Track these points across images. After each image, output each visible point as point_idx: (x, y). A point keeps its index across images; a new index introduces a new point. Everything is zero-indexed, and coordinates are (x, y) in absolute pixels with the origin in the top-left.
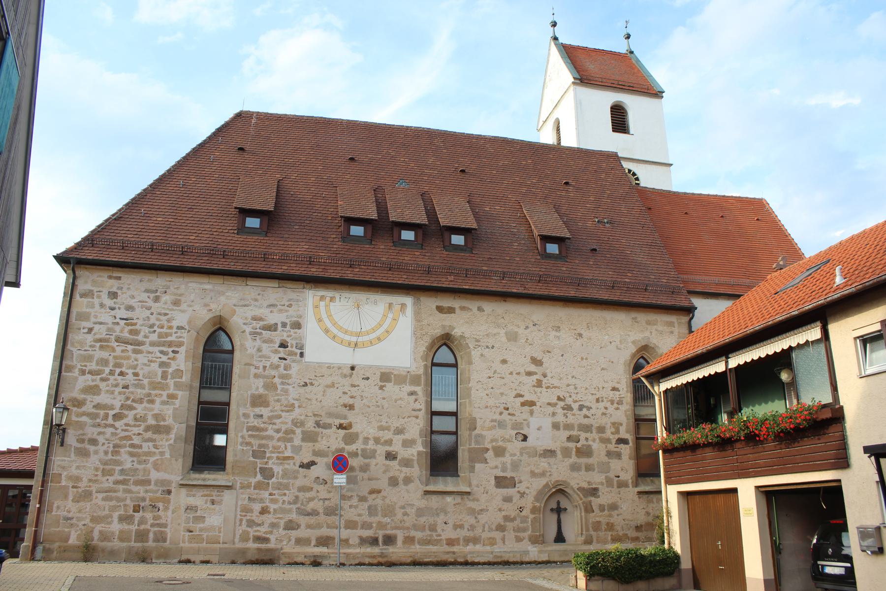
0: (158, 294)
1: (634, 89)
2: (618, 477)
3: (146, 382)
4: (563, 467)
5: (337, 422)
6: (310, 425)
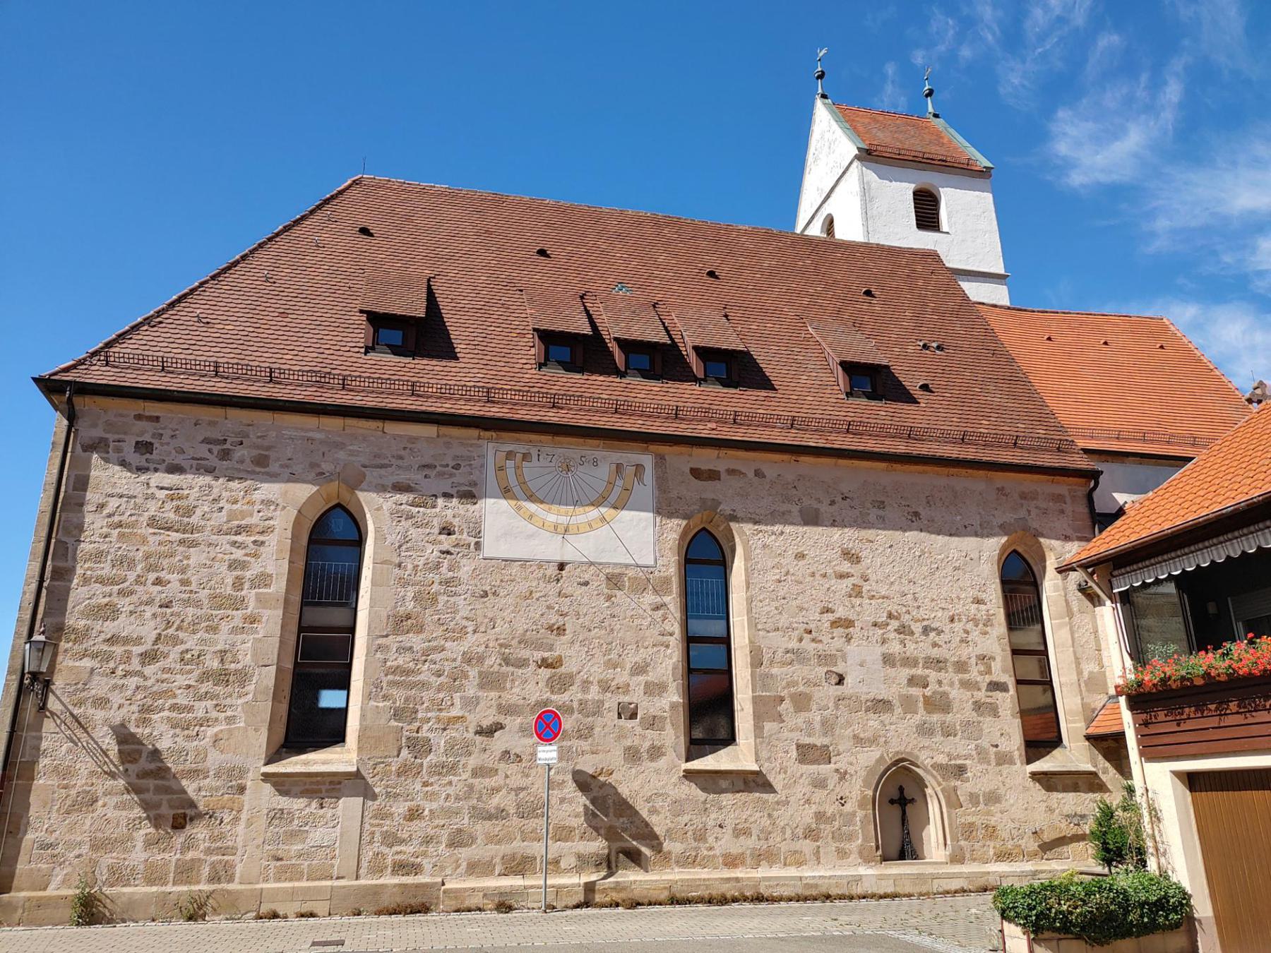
0: (227, 446)
1: (947, 164)
2: (997, 746)
3: (204, 594)
4: (905, 729)
5: (538, 655)
6: (492, 662)
